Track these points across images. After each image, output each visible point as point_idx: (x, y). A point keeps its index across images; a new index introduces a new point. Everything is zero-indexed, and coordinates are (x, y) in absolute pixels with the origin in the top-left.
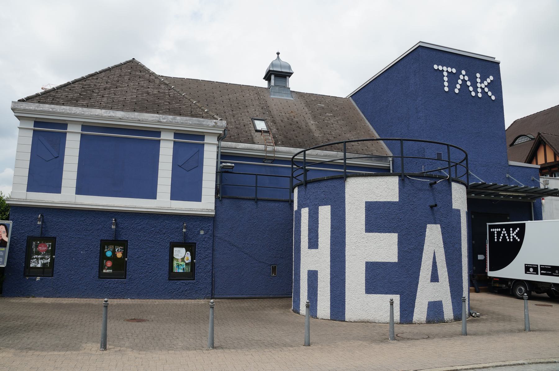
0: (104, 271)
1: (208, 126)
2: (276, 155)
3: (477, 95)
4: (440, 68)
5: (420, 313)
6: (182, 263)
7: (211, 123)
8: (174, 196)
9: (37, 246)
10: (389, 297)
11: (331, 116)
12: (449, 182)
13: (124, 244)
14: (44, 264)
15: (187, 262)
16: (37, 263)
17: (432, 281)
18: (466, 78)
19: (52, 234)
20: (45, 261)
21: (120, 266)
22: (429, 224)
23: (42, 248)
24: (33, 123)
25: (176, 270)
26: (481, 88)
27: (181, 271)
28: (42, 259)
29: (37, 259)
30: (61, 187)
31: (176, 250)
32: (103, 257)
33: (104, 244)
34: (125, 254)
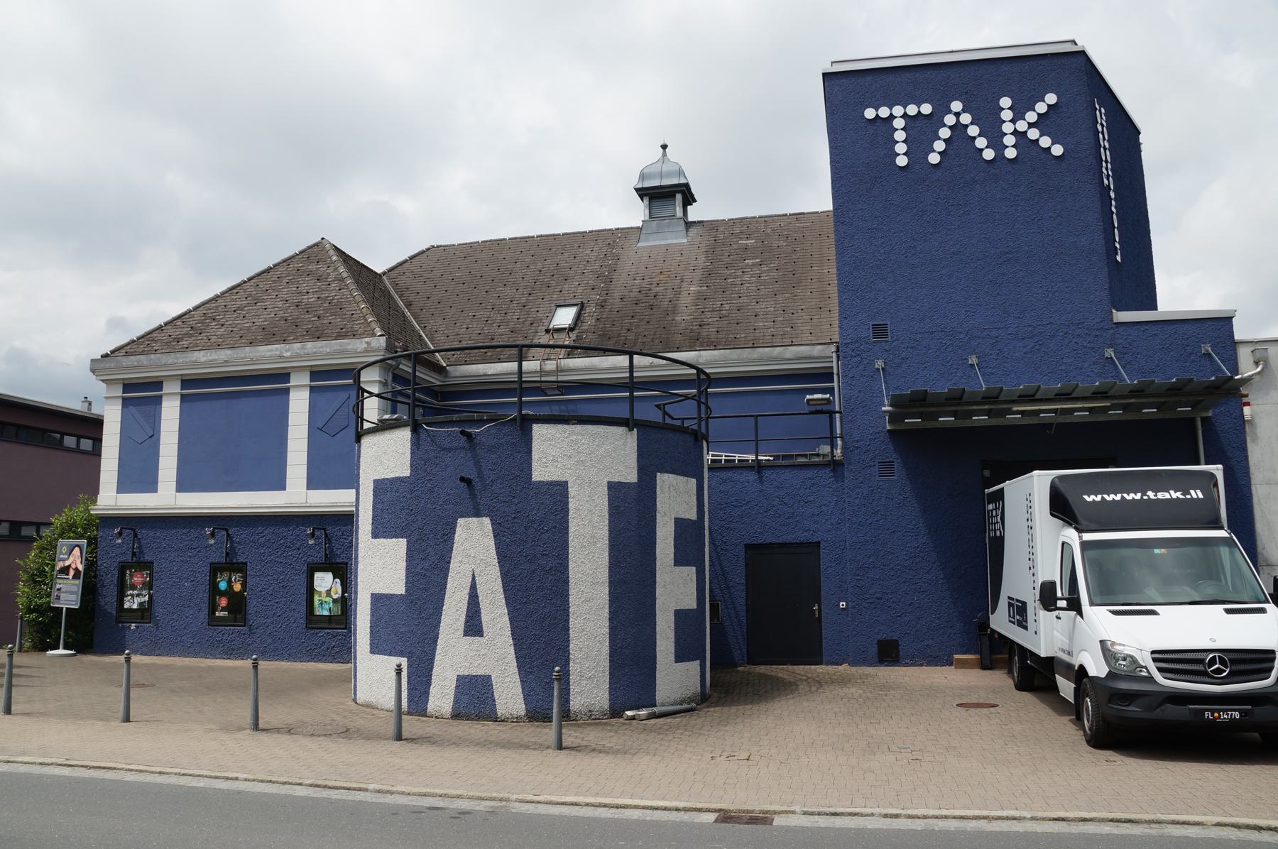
0: (217, 614)
1: (356, 352)
2: (560, 378)
3: (1000, 156)
4: (884, 112)
5: (441, 697)
6: (328, 599)
7: (359, 344)
8: (314, 482)
9: (131, 576)
10: (395, 660)
11: (754, 265)
12: (525, 424)
13: (241, 568)
14: (141, 604)
15: (335, 597)
16: (132, 603)
17: (466, 633)
18: (966, 118)
19: (148, 558)
20: (143, 599)
21: (238, 605)
22: (463, 516)
23: (138, 579)
24: (179, 383)
25: (318, 611)
26: (1015, 133)
27: (326, 613)
28: (138, 595)
29: (132, 596)
30: (157, 483)
31: (317, 575)
32: (214, 590)
33: (215, 570)
34: (244, 585)
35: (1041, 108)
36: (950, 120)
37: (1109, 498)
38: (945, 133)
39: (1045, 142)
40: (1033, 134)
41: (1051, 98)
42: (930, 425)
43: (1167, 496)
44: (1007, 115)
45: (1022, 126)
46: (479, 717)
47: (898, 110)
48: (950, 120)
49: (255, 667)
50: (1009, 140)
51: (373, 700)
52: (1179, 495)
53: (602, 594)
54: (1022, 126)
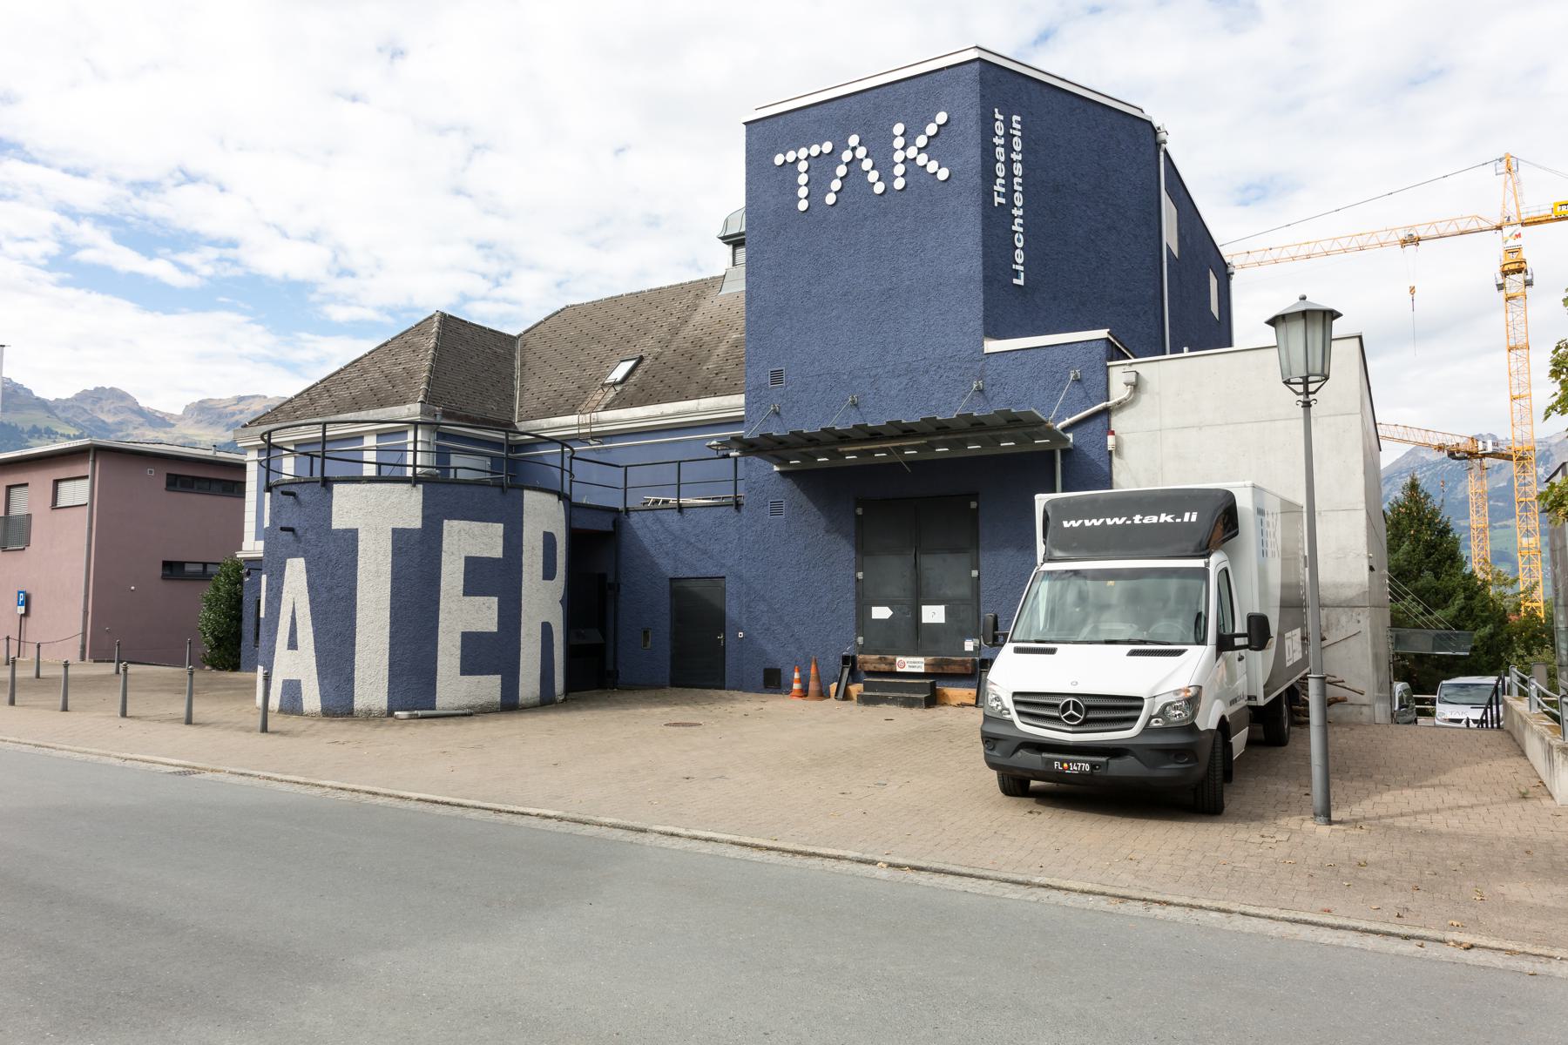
12: (327, 483)
35: (931, 129)
36: (847, 156)
37: (1109, 522)
38: (841, 171)
39: (932, 167)
40: (922, 159)
41: (942, 118)
42: (960, 454)
43: (1155, 519)
44: (899, 142)
45: (912, 152)
46: (292, 713)
47: (803, 153)
48: (847, 156)
49: (191, 674)
50: (899, 170)
51: (907, 710)
52: (1169, 519)
53: (281, 622)
54: (912, 152)
